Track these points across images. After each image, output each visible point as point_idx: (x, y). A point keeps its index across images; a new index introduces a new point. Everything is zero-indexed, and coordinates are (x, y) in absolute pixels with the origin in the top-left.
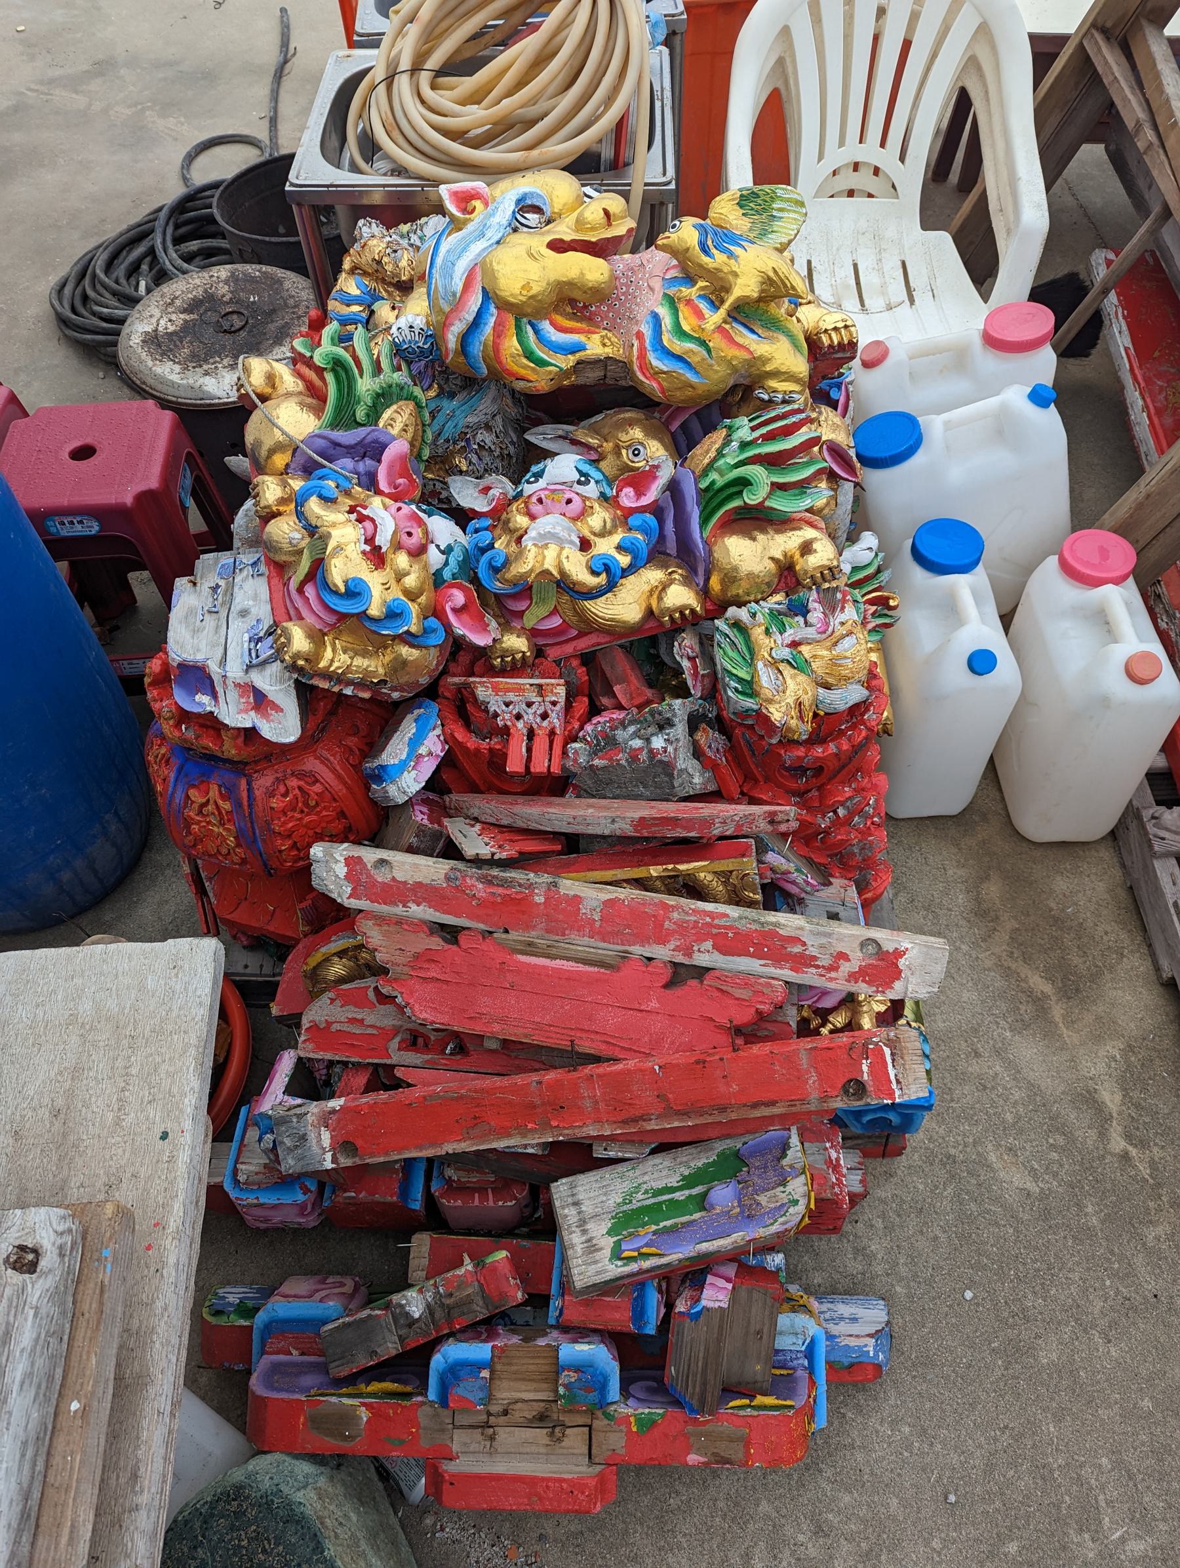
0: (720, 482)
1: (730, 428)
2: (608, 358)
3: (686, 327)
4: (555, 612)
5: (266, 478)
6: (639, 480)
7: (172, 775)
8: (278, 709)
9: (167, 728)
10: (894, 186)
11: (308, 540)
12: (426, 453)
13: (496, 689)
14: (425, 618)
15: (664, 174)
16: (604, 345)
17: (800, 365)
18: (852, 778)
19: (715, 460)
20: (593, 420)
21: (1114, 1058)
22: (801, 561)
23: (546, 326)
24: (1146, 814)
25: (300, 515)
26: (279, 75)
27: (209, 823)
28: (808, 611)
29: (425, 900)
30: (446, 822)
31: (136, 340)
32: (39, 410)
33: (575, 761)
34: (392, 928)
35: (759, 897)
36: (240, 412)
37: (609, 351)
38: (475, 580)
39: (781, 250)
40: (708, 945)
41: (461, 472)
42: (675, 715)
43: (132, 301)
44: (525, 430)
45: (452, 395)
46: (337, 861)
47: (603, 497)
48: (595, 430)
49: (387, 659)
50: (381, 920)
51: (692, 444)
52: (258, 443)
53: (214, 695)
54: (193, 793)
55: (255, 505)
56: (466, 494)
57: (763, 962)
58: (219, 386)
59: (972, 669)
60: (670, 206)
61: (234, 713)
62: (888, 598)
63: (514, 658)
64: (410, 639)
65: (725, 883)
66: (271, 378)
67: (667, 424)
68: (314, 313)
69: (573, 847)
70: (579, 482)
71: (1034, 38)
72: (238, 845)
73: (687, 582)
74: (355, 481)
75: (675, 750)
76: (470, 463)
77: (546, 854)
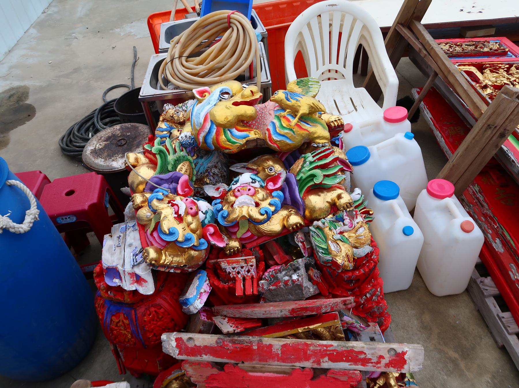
0: (304, 177)
1: (305, 157)
2: (257, 139)
3: (284, 125)
4: (248, 231)
5: (137, 194)
6: (274, 179)
7: (105, 312)
8: (145, 281)
9: (102, 293)
10: (343, 75)
11: (153, 215)
12: (194, 179)
13: (229, 263)
14: (200, 239)
15: (267, 79)
16: (256, 134)
17: (327, 134)
18: (370, 282)
19: (301, 169)
20: (254, 160)
21: (488, 382)
22: (338, 201)
23: (234, 130)
24: (478, 281)
25: (150, 206)
26: (134, 65)
27: (121, 329)
28: (344, 220)
29: (208, 353)
30: (214, 318)
31: (88, 152)
32: (54, 180)
33: (263, 288)
34: (197, 367)
35: (343, 335)
36: (127, 171)
37: (257, 136)
38: (216, 222)
39: (314, 97)
40: (326, 359)
41: (207, 184)
42: (300, 265)
43: (87, 140)
44: (229, 167)
45: (202, 157)
46: (172, 340)
47: (262, 187)
48: (254, 163)
49: (186, 256)
50: (193, 364)
51: (291, 165)
52: (133, 182)
53: (121, 279)
54: (114, 318)
55: (133, 205)
56: (210, 191)
57: (350, 363)
58: (118, 164)
59: (405, 233)
60: (270, 89)
61: (128, 286)
62: (369, 211)
63: (234, 250)
64: (194, 248)
65: (329, 331)
66: (137, 160)
67: (281, 158)
68: (150, 136)
69: (266, 325)
70: (252, 182)
71: (382, 29)
72: (132, 337)
73: (297, 214)
74: (169, 192)
75: (302, 279)
76: (210, 180)
77: (255, 328)
